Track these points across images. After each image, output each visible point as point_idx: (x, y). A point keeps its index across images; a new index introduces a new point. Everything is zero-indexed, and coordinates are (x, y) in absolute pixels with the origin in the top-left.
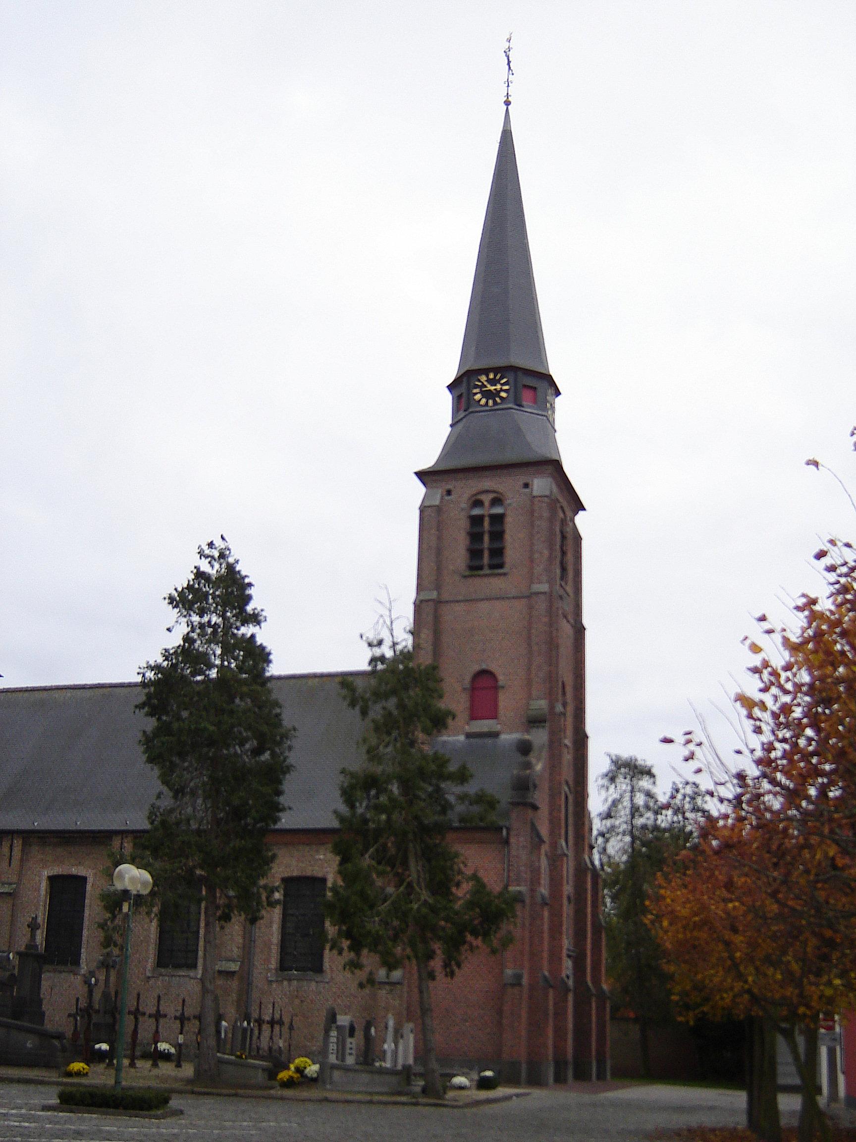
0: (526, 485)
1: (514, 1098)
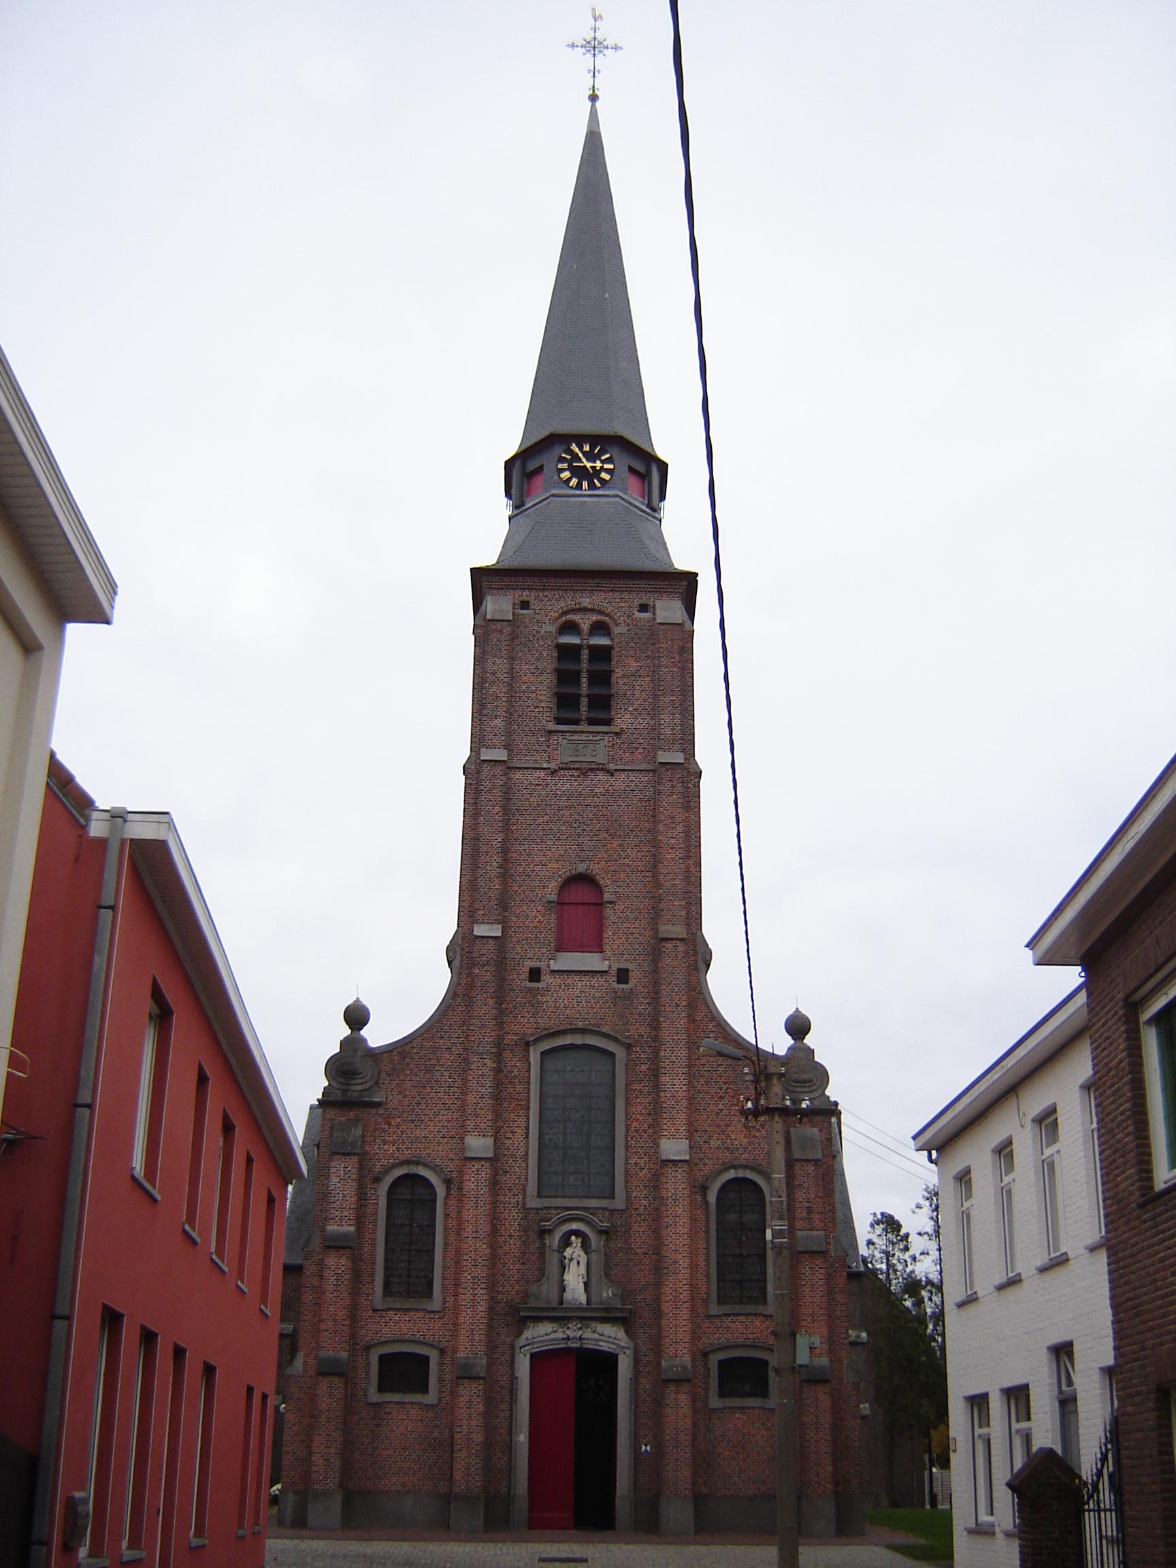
0: (644, 608)
1: (1147, 1283)
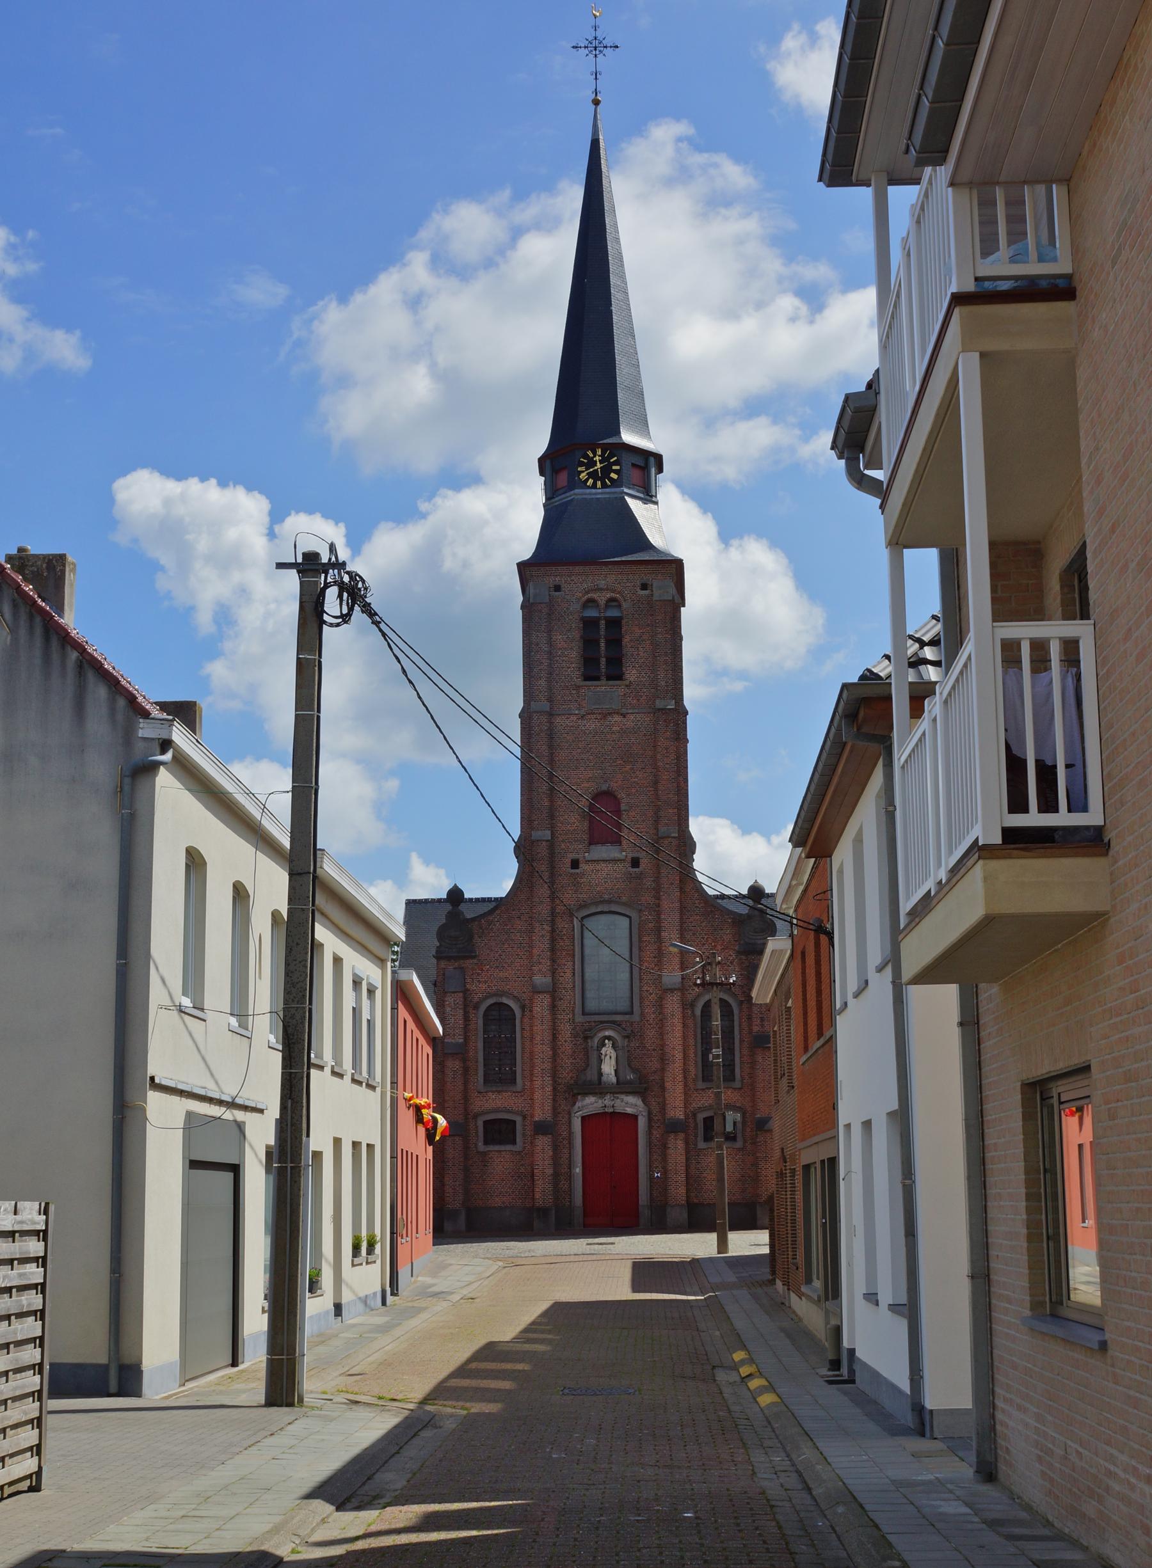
0: (644, 587)
